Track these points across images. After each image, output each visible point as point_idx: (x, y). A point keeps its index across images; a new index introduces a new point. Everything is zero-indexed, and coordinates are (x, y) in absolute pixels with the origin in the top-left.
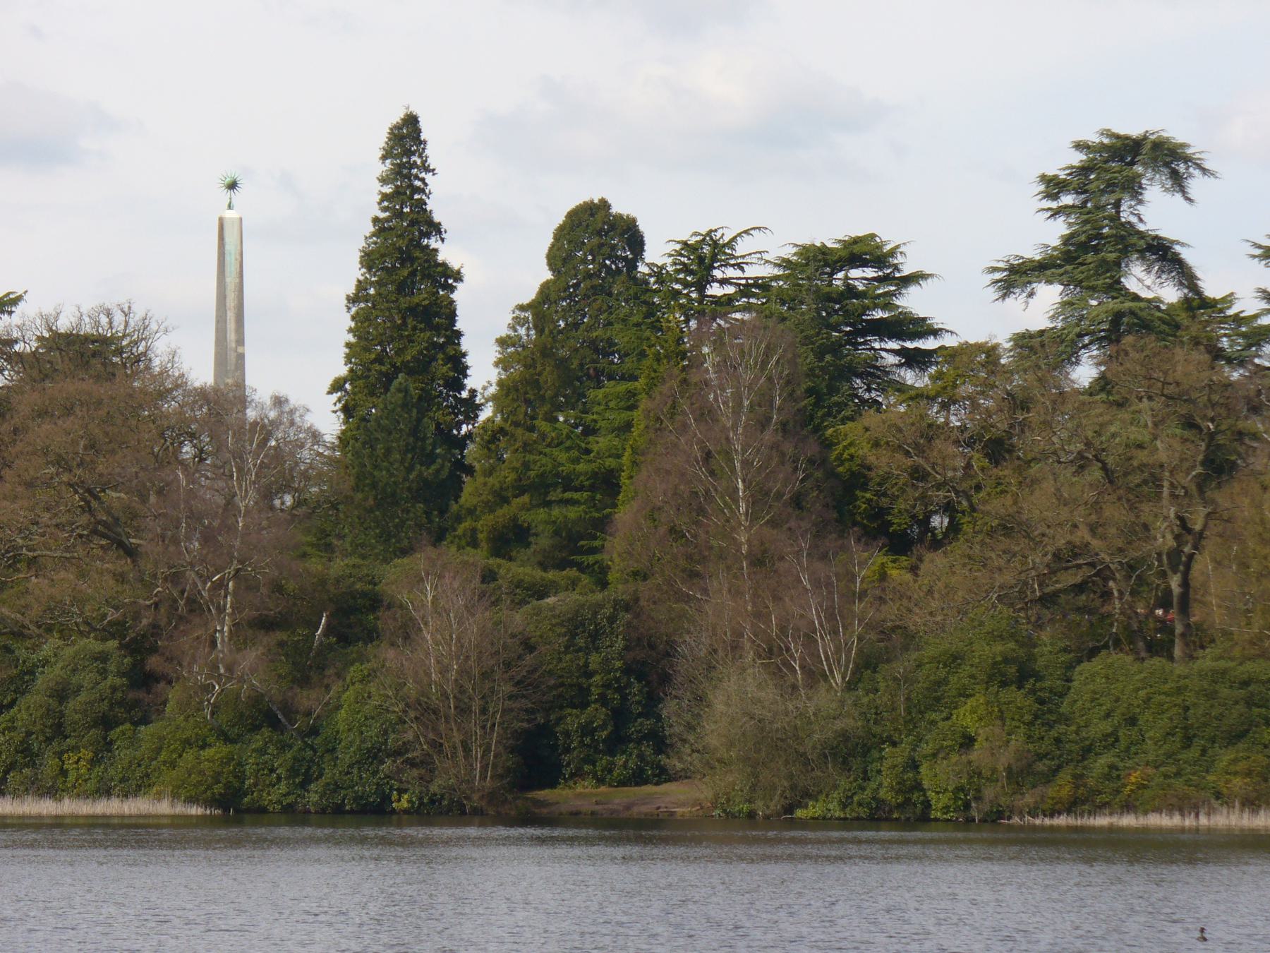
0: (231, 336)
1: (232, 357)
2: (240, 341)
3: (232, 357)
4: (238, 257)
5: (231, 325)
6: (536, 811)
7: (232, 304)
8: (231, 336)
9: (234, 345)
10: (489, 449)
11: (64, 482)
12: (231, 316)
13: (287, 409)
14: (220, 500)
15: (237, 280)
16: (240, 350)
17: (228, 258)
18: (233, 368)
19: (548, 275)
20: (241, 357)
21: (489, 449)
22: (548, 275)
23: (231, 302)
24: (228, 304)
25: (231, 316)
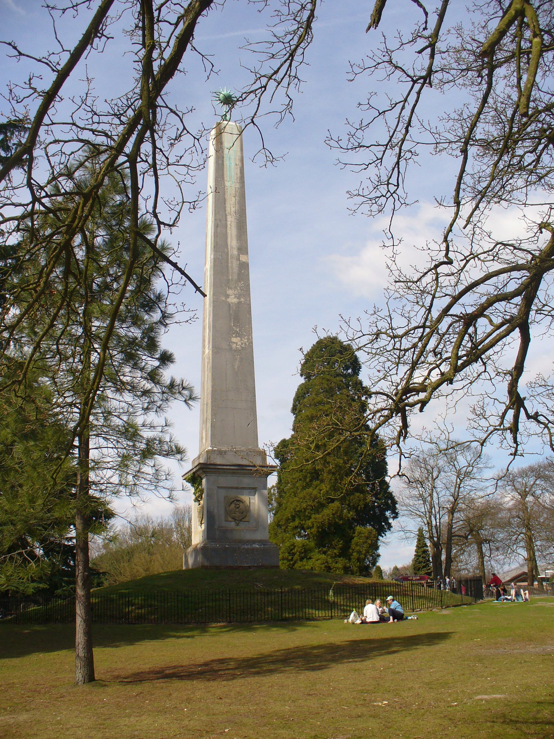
0: (233, 243)
1: (234, 266)
2: (243, 249)
3: (234, 266)
4: (238, 163)
5: (232, 231)
6: (70, 543)
7: (233, 209)
8: (233, 243)
9: (235, 252)
10: (282, 470)
11: (413, 704)
12: (231, 221)
13: (150, 534)
14: (541, 119)
15: (238, 186)
16: (243, 258)
17: (226, 163)
18: (235, 277)
19: (302, 380)
20: (244, 267)
21: (282, 470)
22: (302, 380)
23: (231, 206)
24: (228, 209)
25: (231, 221)
